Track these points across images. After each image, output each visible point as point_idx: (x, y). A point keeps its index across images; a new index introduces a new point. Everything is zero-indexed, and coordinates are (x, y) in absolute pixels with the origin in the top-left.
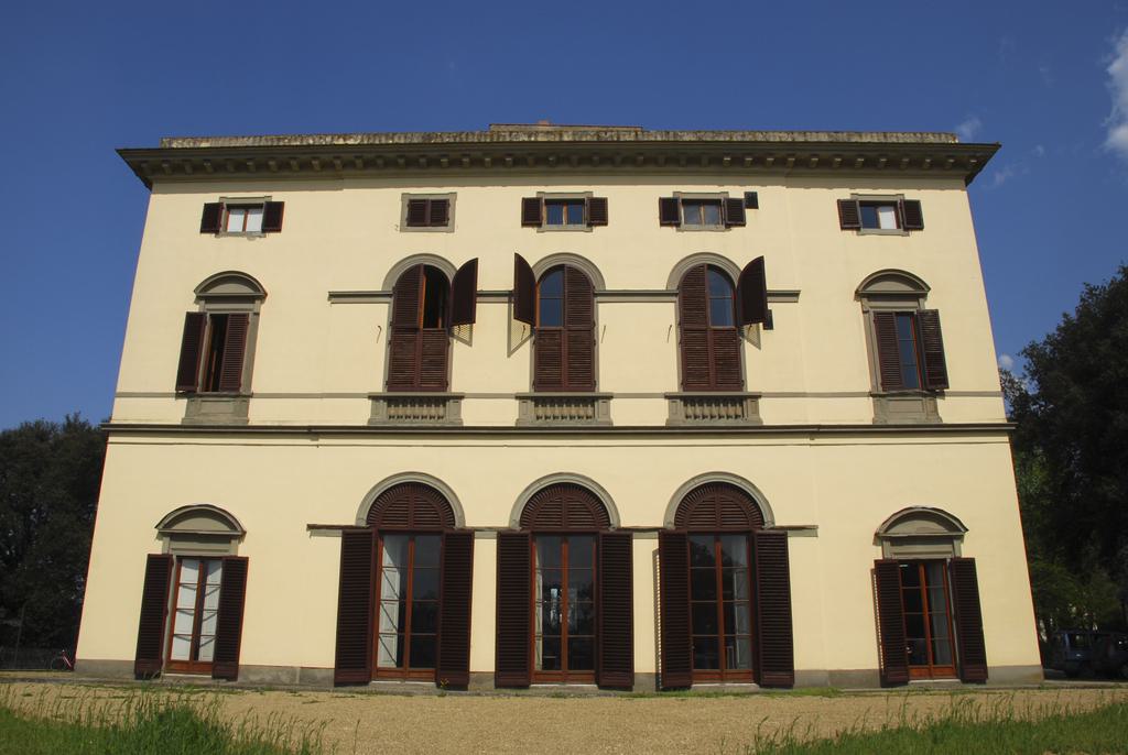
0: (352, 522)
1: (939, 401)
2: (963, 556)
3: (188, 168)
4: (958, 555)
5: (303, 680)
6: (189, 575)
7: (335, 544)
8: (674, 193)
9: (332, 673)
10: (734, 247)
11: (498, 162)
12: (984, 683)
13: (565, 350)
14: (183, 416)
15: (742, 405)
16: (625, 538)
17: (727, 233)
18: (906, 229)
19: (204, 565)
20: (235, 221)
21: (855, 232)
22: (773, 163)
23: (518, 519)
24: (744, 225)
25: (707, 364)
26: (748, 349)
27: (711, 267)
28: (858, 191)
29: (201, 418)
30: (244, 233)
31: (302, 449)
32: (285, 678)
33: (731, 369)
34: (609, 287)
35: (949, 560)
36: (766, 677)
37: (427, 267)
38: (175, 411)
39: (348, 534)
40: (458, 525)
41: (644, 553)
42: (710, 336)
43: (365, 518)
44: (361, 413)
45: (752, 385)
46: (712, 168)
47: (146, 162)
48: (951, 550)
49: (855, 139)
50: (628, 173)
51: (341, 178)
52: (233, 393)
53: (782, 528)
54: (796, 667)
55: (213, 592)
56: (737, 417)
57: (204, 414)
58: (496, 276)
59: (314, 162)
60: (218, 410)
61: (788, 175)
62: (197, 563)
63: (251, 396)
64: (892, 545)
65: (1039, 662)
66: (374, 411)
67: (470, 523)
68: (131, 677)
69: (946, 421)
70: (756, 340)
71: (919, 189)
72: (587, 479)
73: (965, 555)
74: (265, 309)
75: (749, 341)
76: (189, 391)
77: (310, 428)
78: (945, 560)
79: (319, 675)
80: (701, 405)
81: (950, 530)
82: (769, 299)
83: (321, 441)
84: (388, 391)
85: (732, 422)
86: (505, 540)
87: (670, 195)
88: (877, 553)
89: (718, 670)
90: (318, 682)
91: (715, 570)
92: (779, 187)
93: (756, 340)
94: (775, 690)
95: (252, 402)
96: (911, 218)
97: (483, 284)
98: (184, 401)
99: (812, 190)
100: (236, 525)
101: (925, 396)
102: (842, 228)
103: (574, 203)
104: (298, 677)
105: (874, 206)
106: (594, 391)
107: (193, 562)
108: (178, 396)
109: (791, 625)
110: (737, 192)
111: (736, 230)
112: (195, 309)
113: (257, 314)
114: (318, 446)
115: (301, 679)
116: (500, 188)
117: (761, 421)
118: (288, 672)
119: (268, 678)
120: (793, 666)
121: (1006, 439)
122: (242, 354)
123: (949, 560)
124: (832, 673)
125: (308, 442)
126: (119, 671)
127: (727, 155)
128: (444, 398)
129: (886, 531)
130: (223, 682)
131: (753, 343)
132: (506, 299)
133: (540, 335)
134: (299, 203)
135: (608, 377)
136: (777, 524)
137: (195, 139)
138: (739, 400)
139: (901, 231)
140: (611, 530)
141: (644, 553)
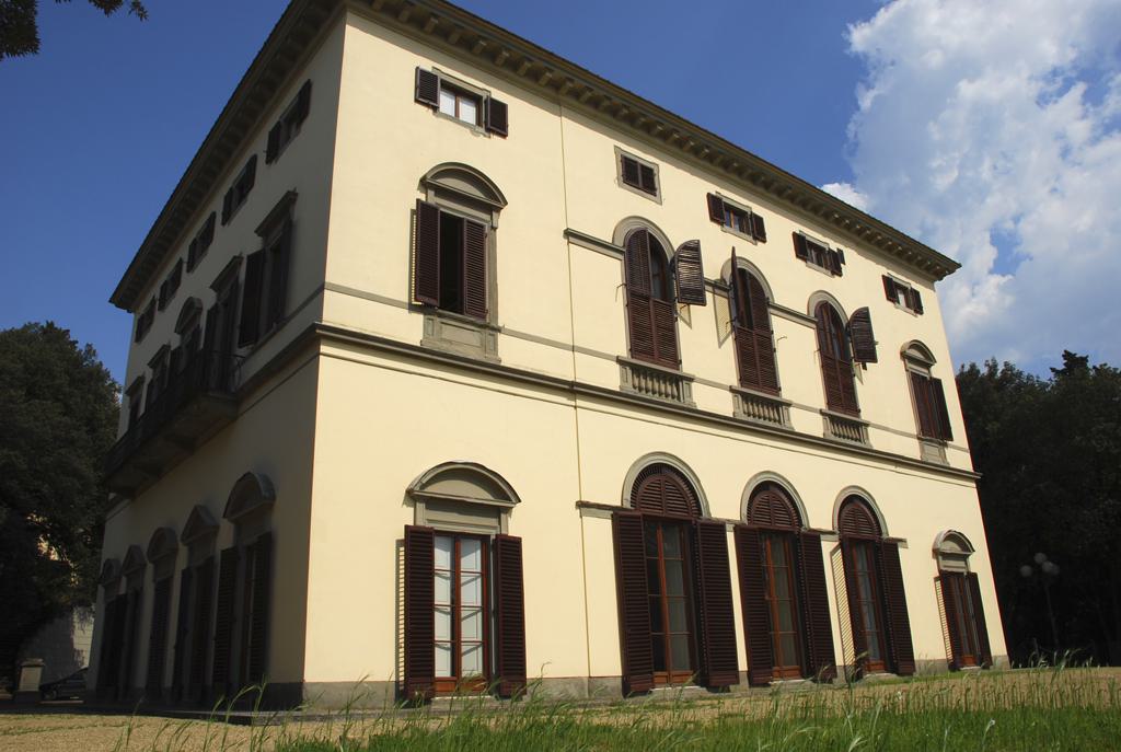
0: (618, 503)
2: (510, 534)
3: (454, 37)
4: (503, 532)
9: (1007, 659)
10: (481, 153)
13: (757, 354)
19: (456, 540)
20: (446, 102)
21: (431, 111)
26: (681, 326)
28: (890, 272)
30: (456, 118)
31: (556, 409)
32: (574, 693)
38: (410, 328)
39: (621, 517)
40: (884, 536)
52: (480, 322)
53: (814, 531)
55: (469, 582)
58: (713, 266)
59: (433, 19)
60: (460, 339)
63: (499, 330)
65: (1006, 653)
69: (506, 363)
72: (784, 479)
73: (512, 532)
74: (504, 220)
77: (573, 384)
78: (489, 536)
83: (580, 402)
86: (738, 529)
87: (429, 69)
88: (407, 516)
89: (665, 674)
93: (722, 338)
96: (494, 120)
101: (940, 444)
108: (412, 308)
110: (834, 246)
113: (494, 229)
118: (576, 685)
121: (974, 485)
123: (493, 537)
125: (893, 468)
129: (424, 486)
131: (685, 322)
134: (522, 112)
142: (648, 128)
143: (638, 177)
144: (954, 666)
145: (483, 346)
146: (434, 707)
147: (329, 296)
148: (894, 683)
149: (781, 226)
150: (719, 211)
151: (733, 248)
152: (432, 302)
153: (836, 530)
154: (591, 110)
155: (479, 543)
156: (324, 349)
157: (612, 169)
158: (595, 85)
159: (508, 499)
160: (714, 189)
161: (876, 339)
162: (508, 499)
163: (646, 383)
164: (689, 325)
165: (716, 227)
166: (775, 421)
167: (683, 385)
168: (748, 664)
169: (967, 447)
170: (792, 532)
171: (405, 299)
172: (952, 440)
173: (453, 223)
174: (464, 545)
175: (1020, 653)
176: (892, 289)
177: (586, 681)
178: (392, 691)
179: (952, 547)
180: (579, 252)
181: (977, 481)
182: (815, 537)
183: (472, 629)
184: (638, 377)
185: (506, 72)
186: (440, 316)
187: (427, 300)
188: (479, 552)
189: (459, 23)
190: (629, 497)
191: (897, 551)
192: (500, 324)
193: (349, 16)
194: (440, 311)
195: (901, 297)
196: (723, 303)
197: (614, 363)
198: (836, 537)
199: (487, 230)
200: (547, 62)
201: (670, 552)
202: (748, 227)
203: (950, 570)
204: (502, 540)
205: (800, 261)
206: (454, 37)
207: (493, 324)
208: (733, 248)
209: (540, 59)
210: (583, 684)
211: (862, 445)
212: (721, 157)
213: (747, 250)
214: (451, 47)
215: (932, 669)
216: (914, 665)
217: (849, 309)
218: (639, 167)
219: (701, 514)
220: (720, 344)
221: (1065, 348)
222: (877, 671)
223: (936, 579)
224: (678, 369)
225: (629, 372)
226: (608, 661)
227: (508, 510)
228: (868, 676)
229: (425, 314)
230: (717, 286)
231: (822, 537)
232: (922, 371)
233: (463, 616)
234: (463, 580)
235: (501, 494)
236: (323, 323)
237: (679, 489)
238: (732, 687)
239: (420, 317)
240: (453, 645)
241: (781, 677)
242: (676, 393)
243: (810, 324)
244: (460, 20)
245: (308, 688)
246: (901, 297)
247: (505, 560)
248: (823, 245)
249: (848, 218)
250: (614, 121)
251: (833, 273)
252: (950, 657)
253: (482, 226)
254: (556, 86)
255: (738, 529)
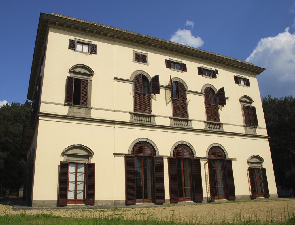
0: (127, 153)
1: (256, 129)
2: (91, 163)
3: (65, 26)
5: (115, 205)
6: (72, 169)
7: (122, 160)
8: (201, 66)
9: (125, 202)
11: (166, 49)
12: (234, 200)
13: (180, 106)
14: (68, 113)
15: (150, 118)
16: (198, 160)
17: (213, 80)
18: (91, 53)
19: (77, 165)
20: (79, 47)
21: (73, 51)
22: (218, 62)
23: (172, 154)
24: (96, 54)
25: (212, 114)
27: (211, 88)
28: (237, 74)
29: (74, 114)
30: (82, 52)
31: (109, 128)
32: (110, 204)
33: (148, 106)
34: (189, 89)
35: (86, 164)
36: (157, 201)
37: (143, 75)
38: (65, 111)
39: (127, 157)
40: (227, 158)
41: (166, 162)
42: (212, 106)
43: (131, 151)
44: (127, 118)
45: (153, 113)
46: (124, 41)
47: (51, 20)
48: (88, 160)
49: (77, 20)
50: (190, 58)
51: (114, 41)
53: (230, 159)
54: (236, 195)
56: (149, 122)
57: (75, 113)
58: (164, 81)
59: (72, 26)
60: (79, 112)
61: (224, 67)
62: (75, 165)
63: (91, 108)
64: (251, 164)
66: (131, 118)
67: (198, 156)
68: (55, 206)
70: (155, 98)
71: (232, 72)
72: (188, 143)
73: (264, 167)
74: (94, 78)
75: (153, 98)
76: (69, 104)
77: (113, 121)
78: (260, 168)
79: (121, 202)
80: (139, 117)
81: (260, 161)
82: (160, 88)
83: (116, 126)
84: (174, 116)
85: (147, 123)
86: (169, 159)
88: (62, 159)
89: (142, 199)
90: (121, 205)
91: (181, 169)
92: (222, 70)
94: (198, 203)
95: (92, 110)
96: (93, 50)
97: (161, 83)
98: (67, 107)
99: (228, 72)
100: (91, 152)
101: (253, 128)
102: (69, 49)
103: (208, 71)
104: (114, 204)
105: (240, 78)
106: (151, 114)
107: (73, 164)
108: (65, 105)
109: (202, 184)
110: (214, 69)
111: (93, 55)
112: (69, 75)
113: (91, 81)
114: (115, 127)
115: (115, 204)
116: (159, 55)
117: (224, 131)
119: (104, 204)
120: (269, 193)
121: (268, 140)
122: (87, 94)
123: (86, 164)
124: (242, 196)
125: (233, 136)
126: (50, 204)
127: (214, 59)
128: (220, 125)
129: (66, 152)
130: (89, 206)
131: (220, 110)
132: (164, 88)
133: (174, 100)
134: (102, 46)
135: (155, 110)
136: (229, 158)
137: (68, 17)
138: (187, 121)
139: (89, 53)
140: (194, 158)
141: (166, 162)
142: (143, 43)
143: (141, 58)
144: (253, 197)
145: (86, 113)
146: (67, 207)
147: (42, 105)
148: (227, 202)
149: (192, 66)
150: (169, 64)
151: (170, 76)
152: (71, 103)
153: (207, 157)
154: (160, 50)
155: (84, 165)
156: (40, 118)
157: (132, 57)
158: (110, 31)
159: (91, 154)
160: (235, 74)
161: (226, 96)
162: (91, 154)
163: (213, 126)
164: (156, 100)
165: (200, 76)
166: (218, 129)
167: (189, 122)
168: (126, 198)
169: (265, 127)
170: (190, 158)
171: (63, 102)
172: (258, 126)
173: (78, 81)
174: (79, 166)
175: (281, 194)
176: (237, 80)
177: (114, 201)
178: (250, 198)
179: (257, 160)
180: (119, 84)
181: (269, 138)
182: (198, 160)
183: (81, 187)
184: (209, 125)
185: (97, 35)
186: (73, 106)
187: (69, 103)
188: (84, 167)
189: (80, 25)
190: (208, 156)
191: (231, 162)
192: (92, 107)
193: (50, 29)
194: (73, 105)
195: (242, 82)
196: (169, 92)
197: (203, 122)
198: (207, 159)
199: (89, 81)
200: (109, 31)
201: (186, 169)
202: (180, 68)
203: (253, 167)
204: (89, 164)
205: (236, 84)
206: (65, 26)
207: (89, 107)
208: (170, 76)
209: (106, 31)
210: (113, 203)
211: (220, 131)
212: (169, 48)
213: (176, 74)
214: (80, 32)
215: (243, 198)
216: (269, 195)
217: (218, 88)
218: (141, 55)
219: (156, 155)
220: (167, 104)
221: (198, 66)
222: (222, 199)
223: (248, 170)
224: (219, 122)
225: (173, 120)
226: (121, 195)
227: (262, 163)
228: (216, 200)
229: (69, 106)
230: (166, 88)
231: (201, 159)
232: (248, 105)
233: (78, 184)
234: (78, 175)
235: (89, 153)
236: (40, 112)
237: (220, 152)
238: (163, 203)
239: (68, 107)
240: (75, 191)
241: (219, 199)
242: (219, 128)
243: (202, 95)
244: (102, 29)
245: (34, 202)
246: (242, 82)
247: (90, 170)
248: (210, 69)
249: (218, 60)
250: (132, 43)
251: (213, 78)
252: (251, 194)
253: (87, 80)
254: (112, 36)
255: (169, 159)
